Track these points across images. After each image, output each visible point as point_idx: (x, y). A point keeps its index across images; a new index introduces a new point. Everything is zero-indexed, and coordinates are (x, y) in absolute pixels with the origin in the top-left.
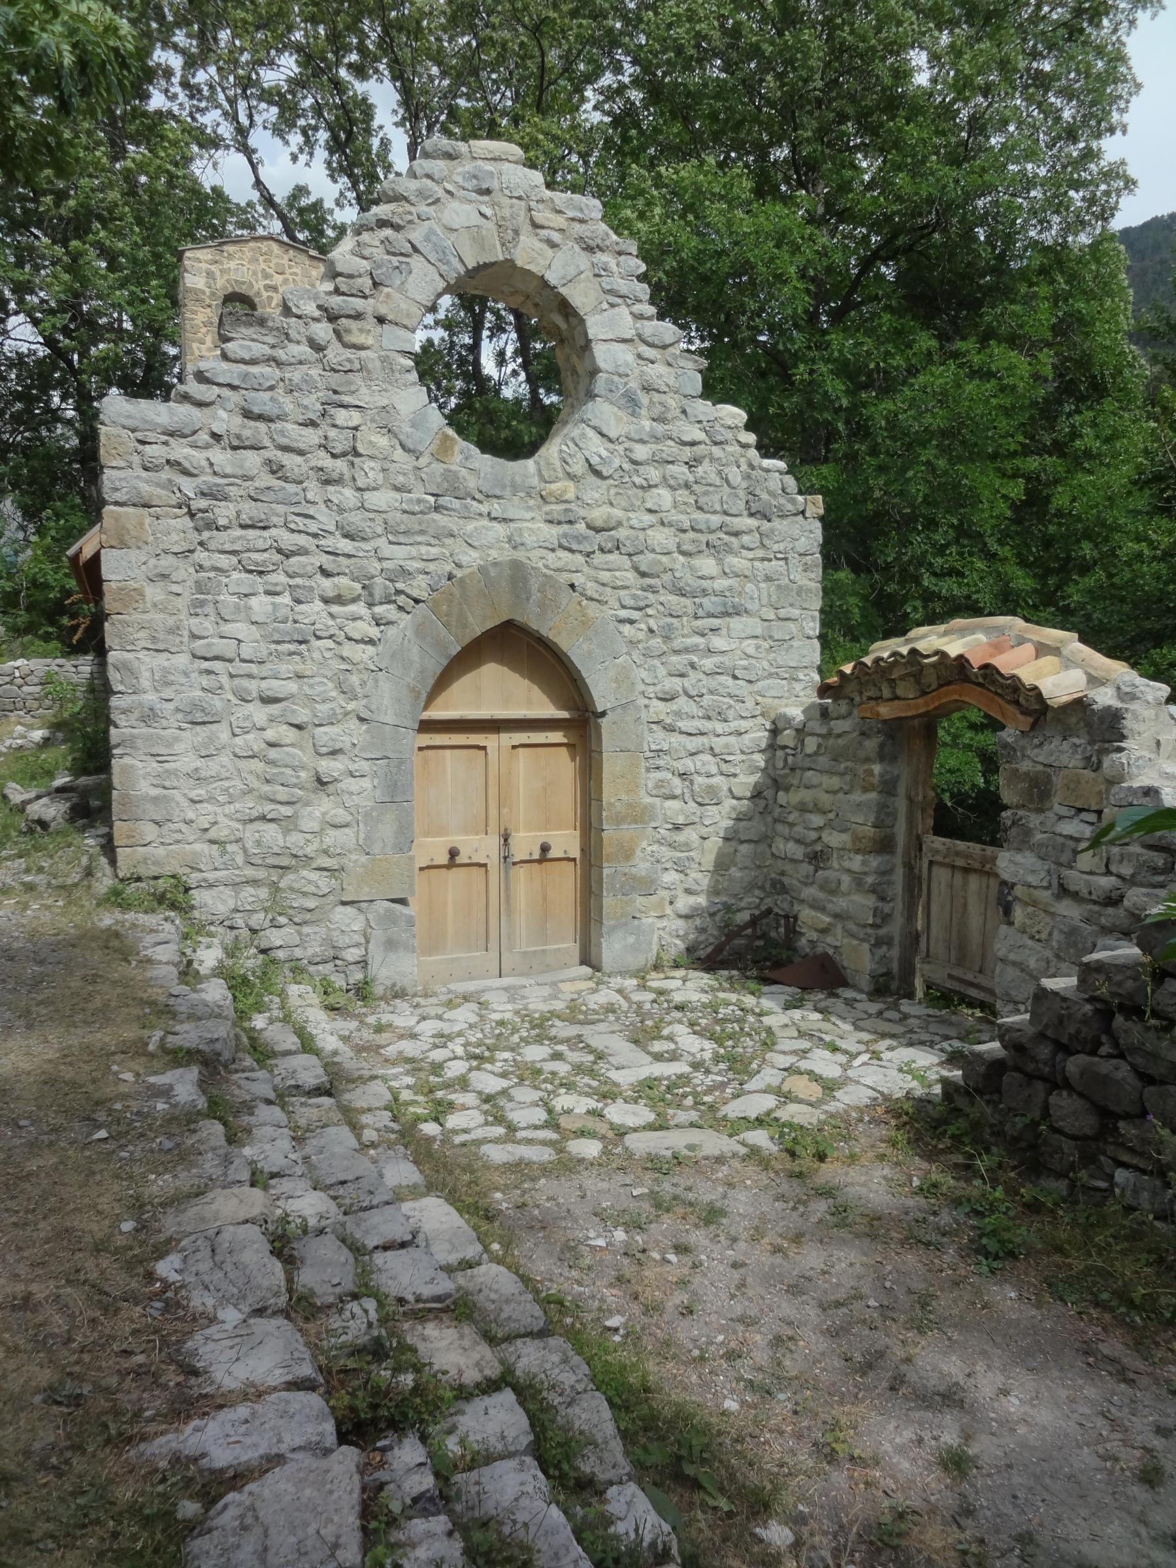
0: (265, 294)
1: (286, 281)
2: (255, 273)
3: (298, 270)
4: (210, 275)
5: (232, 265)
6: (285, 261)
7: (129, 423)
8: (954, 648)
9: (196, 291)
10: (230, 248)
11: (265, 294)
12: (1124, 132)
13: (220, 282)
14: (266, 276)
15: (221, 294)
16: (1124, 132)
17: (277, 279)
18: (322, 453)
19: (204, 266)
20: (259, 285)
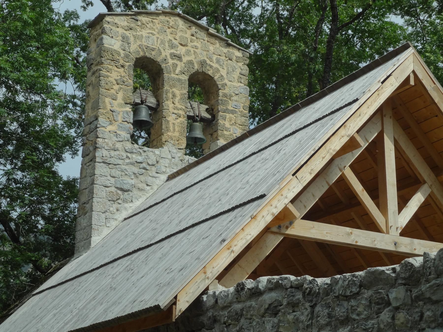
0: (171, 62)
1: (188, 53)
2: (162, 42)
3: (198, 45)
4: (125, 39)
5: (144, 33)
6: (188, 35)
7: (90, 160)
8: (360, 274)
9: (112, 52)
10: (143, 19)
11: (171, 62)
12: (92, 5)
13: (133, 47)
14: (172, 46)
15: (133, 57)
16: (92, 5)
17: (181, 50)
18: (127, 159)
19: (120, 30)
20: (166, 53)
